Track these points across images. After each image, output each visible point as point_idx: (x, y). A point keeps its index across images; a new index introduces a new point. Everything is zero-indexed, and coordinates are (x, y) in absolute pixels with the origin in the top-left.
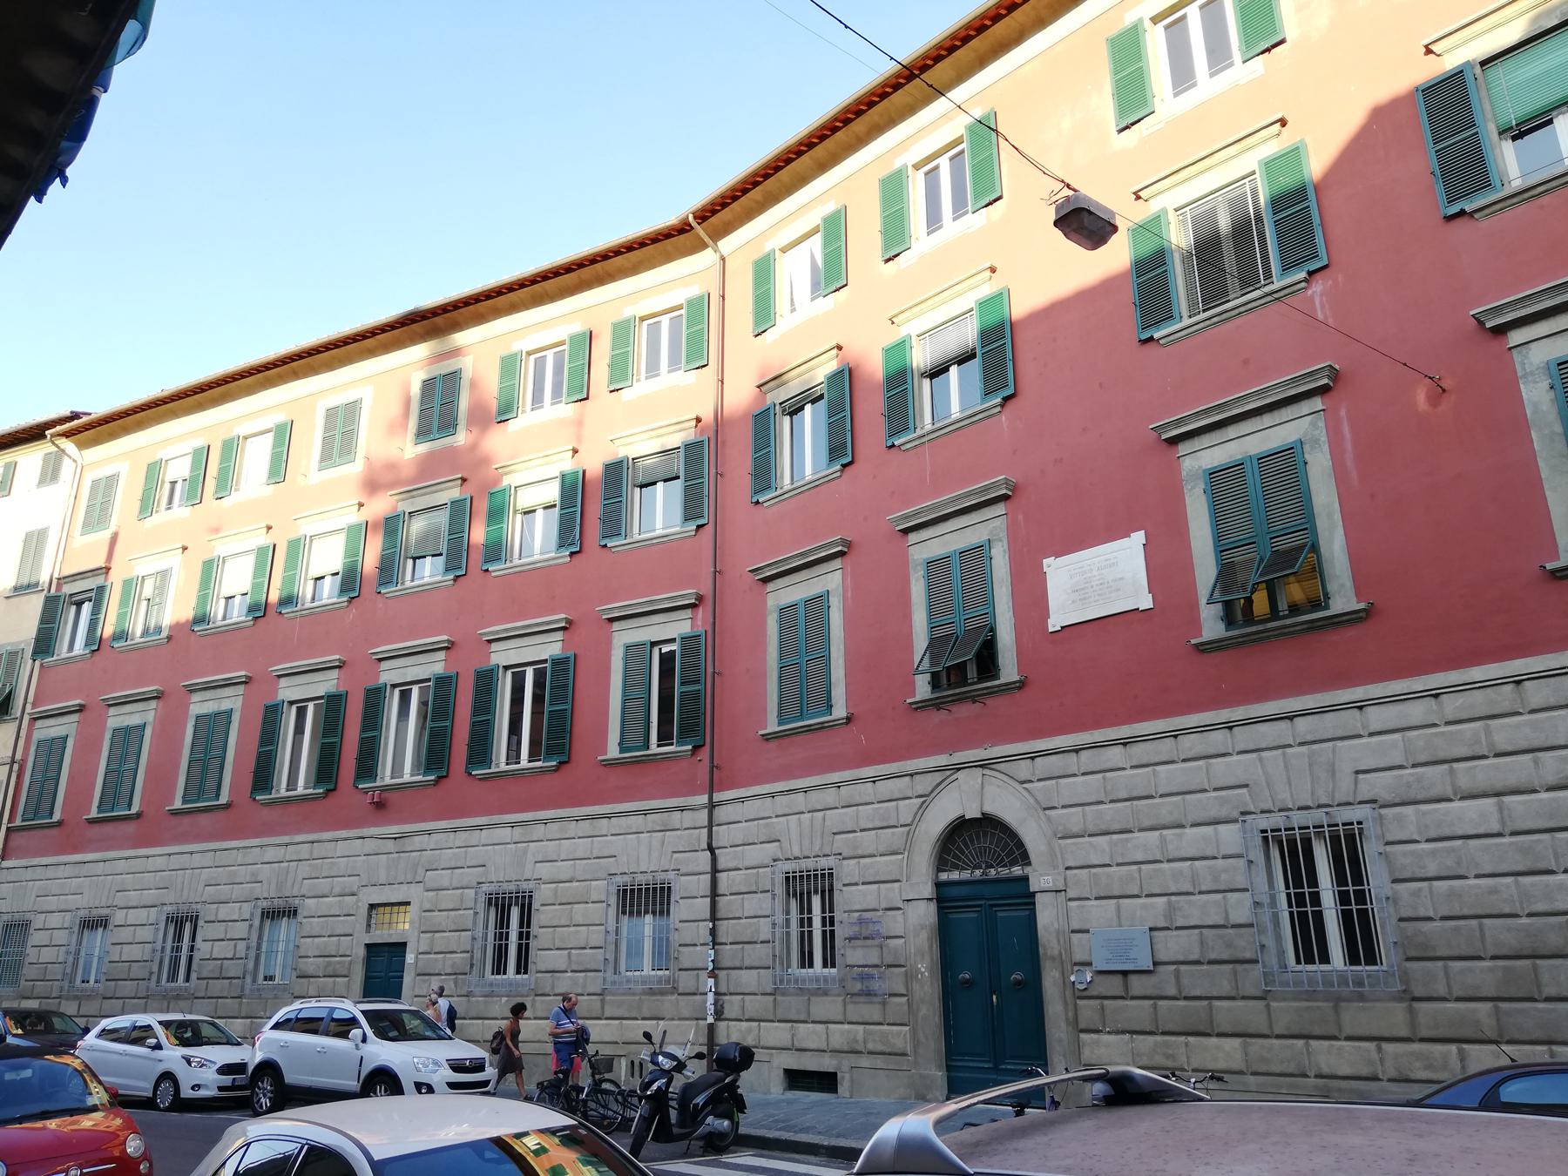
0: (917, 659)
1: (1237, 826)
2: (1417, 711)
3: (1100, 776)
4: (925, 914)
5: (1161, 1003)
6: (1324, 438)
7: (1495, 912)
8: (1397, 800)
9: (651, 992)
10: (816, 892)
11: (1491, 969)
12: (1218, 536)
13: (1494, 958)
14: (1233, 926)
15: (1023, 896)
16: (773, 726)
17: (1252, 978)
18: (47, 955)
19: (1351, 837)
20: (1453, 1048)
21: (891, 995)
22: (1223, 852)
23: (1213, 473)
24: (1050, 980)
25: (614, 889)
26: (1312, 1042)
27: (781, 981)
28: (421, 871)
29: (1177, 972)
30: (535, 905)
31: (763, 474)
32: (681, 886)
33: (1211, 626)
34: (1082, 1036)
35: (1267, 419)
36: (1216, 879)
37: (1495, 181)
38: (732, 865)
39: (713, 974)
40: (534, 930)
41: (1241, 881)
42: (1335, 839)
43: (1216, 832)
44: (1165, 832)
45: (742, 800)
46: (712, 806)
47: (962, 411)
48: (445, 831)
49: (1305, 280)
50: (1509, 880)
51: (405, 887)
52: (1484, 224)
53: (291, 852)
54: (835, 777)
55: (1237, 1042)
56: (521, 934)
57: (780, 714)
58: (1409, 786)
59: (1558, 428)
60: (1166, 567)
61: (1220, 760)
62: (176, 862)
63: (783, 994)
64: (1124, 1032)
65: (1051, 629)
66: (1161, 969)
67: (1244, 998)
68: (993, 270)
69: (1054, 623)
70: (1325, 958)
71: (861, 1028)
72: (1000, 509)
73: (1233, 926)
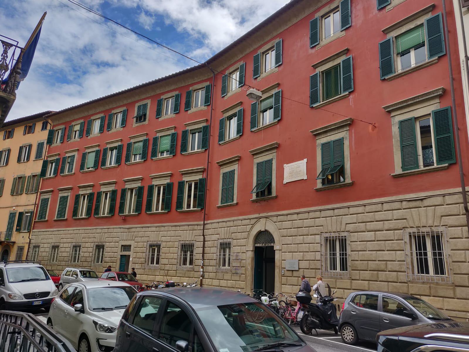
0: (318, 175)
1: (319, 236)
2: (360, 209)
3: (292, 221)
4: (250, 255)
6: (348, 137)
7: (371, 260)
8: (354, 231)
9: (188, 271)
11: (369, 273)
12: (323, 161)
13: (370, 271)
16: (220, 205)
18: (44, 254)
19: (438, 237)
21: (242, 274)
24: (277, 271)
25: (180, 245)
28: (134, 237)
30: (161, 247)
31: (222, 136)
32: (197, 244)
33: (319, 185)
34: (282, 285)
36: (314, 249)
38: (208, 240)
39: (202, 268)
40: (161, 254)
41: (319, 250)
42: (433, 237)
44: (304, 236)
45: (212, 223)
46: (204, 224)
47: (403, 69)
48: (140, 227)
49: (348, 94)
51: (130, 241)
53: (104, 231)
54: (233, 218)
56: (152, 254)
57: (221, 202)
58: (357, 228)
60: (310, 169)
62: (76, 232)
63: (218, 273)
64: (291, 285)
65: (284, 183)
66: (300, 270)
69: (285, 181)
70: (427, 272)
71: (234, 282)
73: (317, 260)
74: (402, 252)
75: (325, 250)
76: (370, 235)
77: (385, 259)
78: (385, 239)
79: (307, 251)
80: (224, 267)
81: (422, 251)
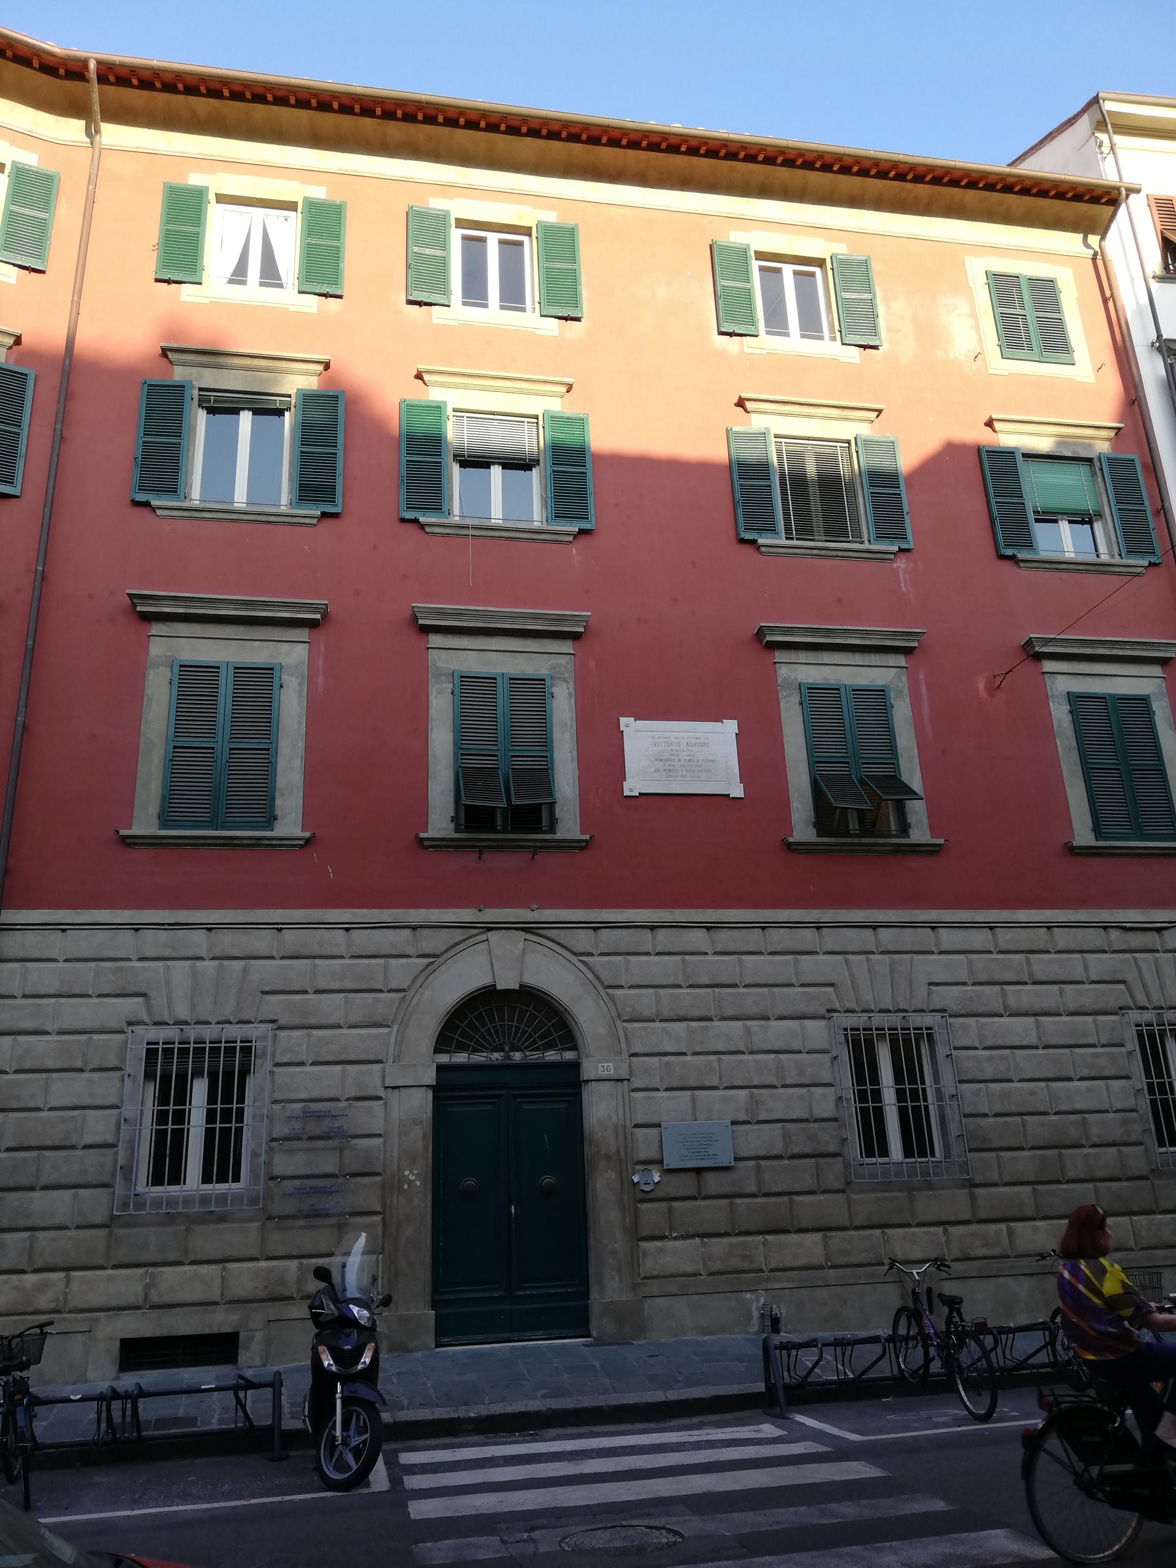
1: (823, 1022)
2: (979, 939)
3: (678, 958)
5: (738, 1201)
6: (906, 692)
8: (963, 1012)
10: (198, 1073)
12: (811, 749)
14: (816, 1120)
15: (569, 1083)
17: (833, 1172)
20: (1003, 1226)
22: (808, 1047)
23: (466, 678)
24: (603, 1187)
26: (888, 1231)
27: (125, 1206)
29: (758, 1167)
33: (803, 830)
34: (643, 1244)
35: (858, 658)
37: (181, 491)
41: (826, 1077)
43: (803, 1027)
44: (749, 1023)
50: (1043, 1084)
52: (1024, 573)
55: (818, 1237)
59: (1074, 743)
61: (807, 957)
64: (693, 1236)
67: (825, 1192)
68: (570, 388)
70: (884, 1152)
72: (567, 646)
73: (816, 1120)
74: (1123, 1083)
75: (142, 1105)
76: (1020, 1028)
77: (1078, 1107)
78: (1072, 1042)
79: (768, 1082)
80: (177, 1188)
81: (171, 1107)
